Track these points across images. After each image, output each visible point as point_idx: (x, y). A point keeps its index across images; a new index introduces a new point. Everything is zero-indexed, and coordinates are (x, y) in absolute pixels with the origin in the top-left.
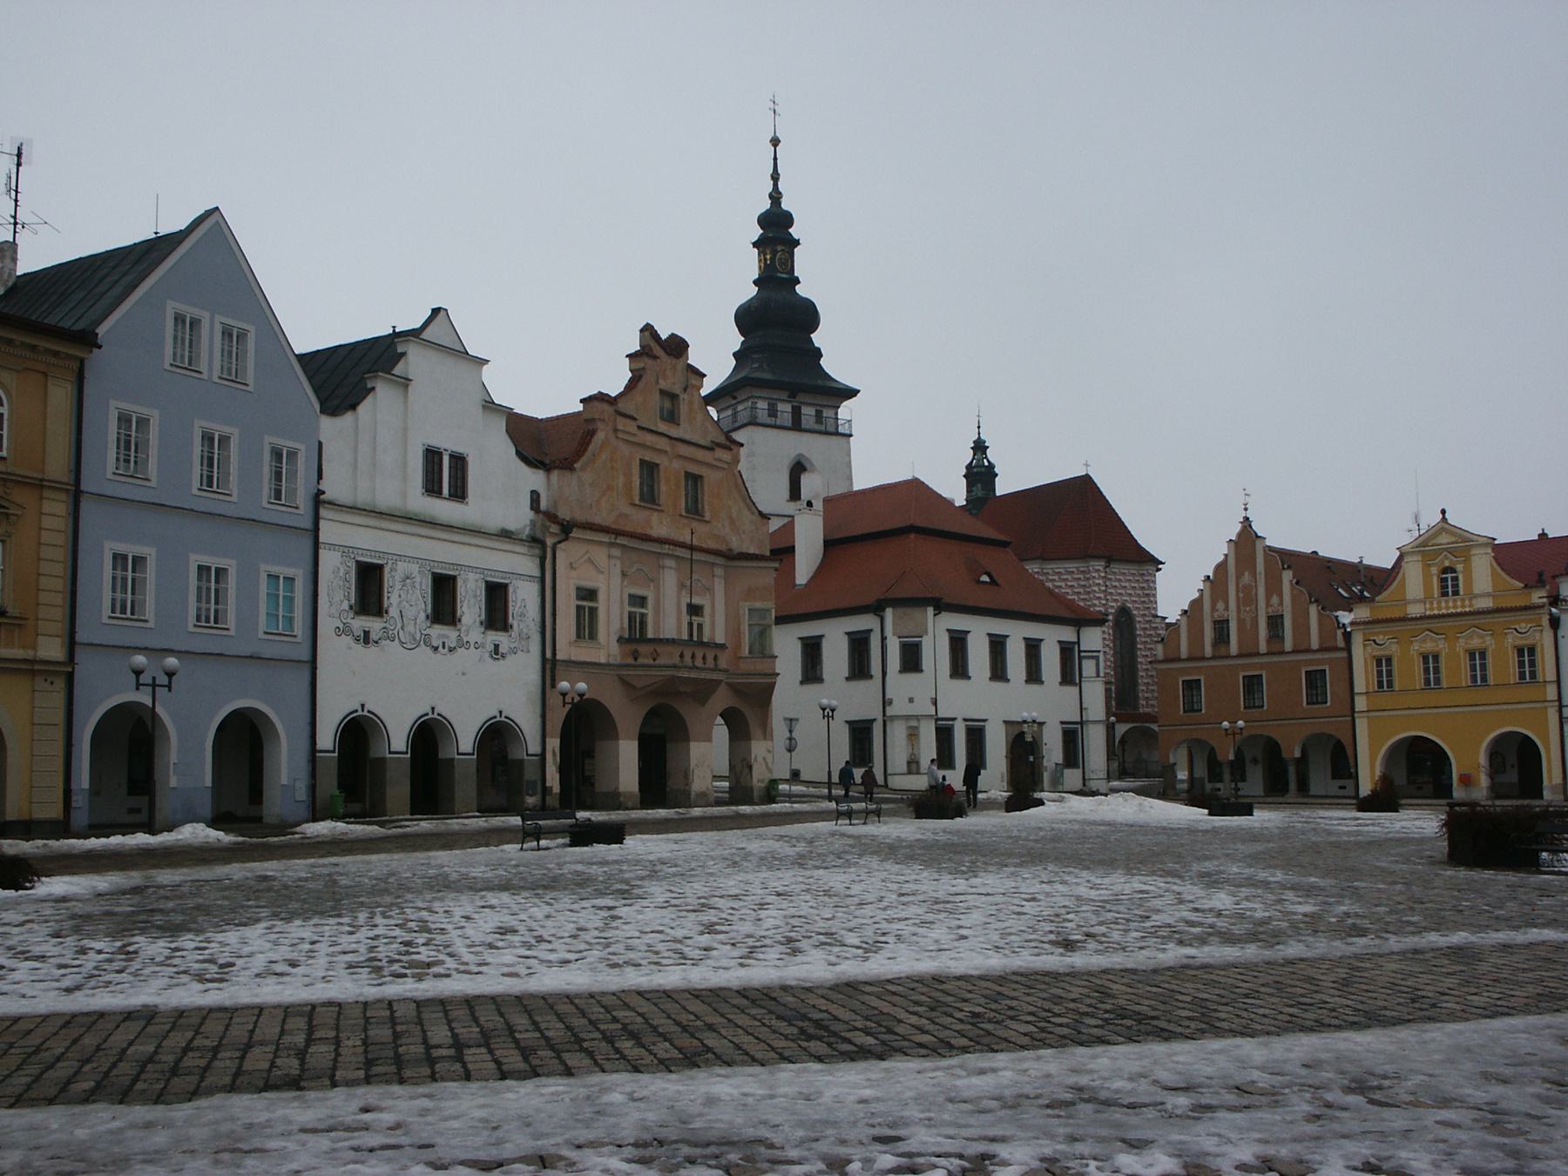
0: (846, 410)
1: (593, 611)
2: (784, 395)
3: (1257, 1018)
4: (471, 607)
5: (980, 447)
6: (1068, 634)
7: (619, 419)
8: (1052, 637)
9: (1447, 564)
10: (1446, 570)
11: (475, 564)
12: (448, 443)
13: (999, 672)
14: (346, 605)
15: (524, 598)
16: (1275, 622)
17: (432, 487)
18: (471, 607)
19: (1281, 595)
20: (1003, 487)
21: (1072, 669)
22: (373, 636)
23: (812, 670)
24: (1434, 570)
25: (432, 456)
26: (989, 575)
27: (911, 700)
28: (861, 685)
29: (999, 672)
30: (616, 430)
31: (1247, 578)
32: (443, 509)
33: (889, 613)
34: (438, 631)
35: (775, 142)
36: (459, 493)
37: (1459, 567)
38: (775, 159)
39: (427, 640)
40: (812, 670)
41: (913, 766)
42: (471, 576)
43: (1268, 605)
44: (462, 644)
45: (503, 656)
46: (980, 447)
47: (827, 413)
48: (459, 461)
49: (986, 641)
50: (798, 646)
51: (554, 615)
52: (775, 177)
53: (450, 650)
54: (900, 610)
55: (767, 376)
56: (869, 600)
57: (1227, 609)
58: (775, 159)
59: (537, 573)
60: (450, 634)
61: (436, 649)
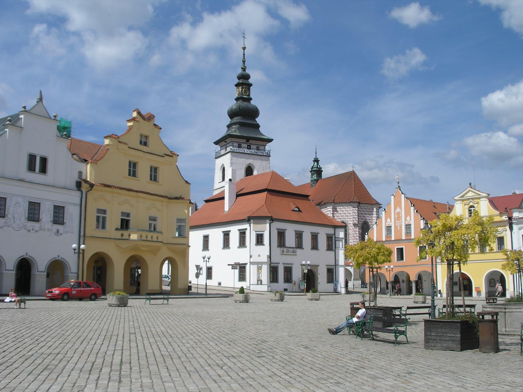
0: (269, 147)
1: (104, 218)
2: (244, 141)
3: (122, 325)
4: (46, 214)
5: (316, 161)
6: (331, 231)
7: (120, 144)
8: (323, 233)
9: (471, 204)
10: (471, 207)
11: (48, 200)
12: (39, 152)
13: (315, 247)
14: (50, 220)
15: (72, 214)
16: (408, 226)
17: (31, 168)
18: (46, 214)
19: (410, 217)
20: (324, 175)
21: (332, 243)
22: (60, 232)
23: (226, 244)
24: (467, 207)
25: (32, 158)
26: (298, 208)
27: (259, 256)
28: (242, 250)
29: (315, 247)
30: (118, 149)
31: (398, 210)
32: (36, 177)
33: (252, 221)
34: (31, 224)
35: (244, 48)
36: (43, 170)
37: (475, 205)
38: (244, 54)
39: (25, 227)
40: (226, 244)
41: (260, 282)
42: (47, 203)
43: (406, 220)
44: (41, 229)
45: (61, 234)
46: (316, 161)
47: (261, 148)
48: (44, 161)
49: (294, 233)
50: (222, 234)
51: (85, 219)
52: (244, 62)
53: (36, 231)
54: (256, 221)
55: (238, 134)
56: (245, 217)
57: (391, 222)
58: (244, 54)
59: (78, 202)
60: (36, 225)
61: (29, 231)
